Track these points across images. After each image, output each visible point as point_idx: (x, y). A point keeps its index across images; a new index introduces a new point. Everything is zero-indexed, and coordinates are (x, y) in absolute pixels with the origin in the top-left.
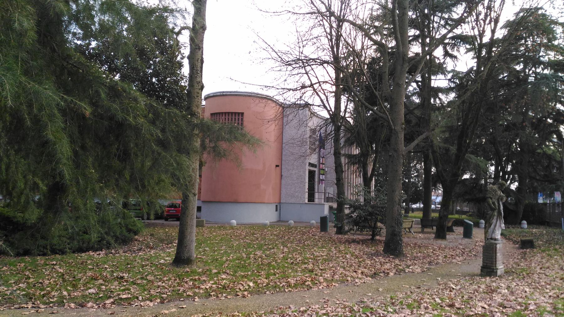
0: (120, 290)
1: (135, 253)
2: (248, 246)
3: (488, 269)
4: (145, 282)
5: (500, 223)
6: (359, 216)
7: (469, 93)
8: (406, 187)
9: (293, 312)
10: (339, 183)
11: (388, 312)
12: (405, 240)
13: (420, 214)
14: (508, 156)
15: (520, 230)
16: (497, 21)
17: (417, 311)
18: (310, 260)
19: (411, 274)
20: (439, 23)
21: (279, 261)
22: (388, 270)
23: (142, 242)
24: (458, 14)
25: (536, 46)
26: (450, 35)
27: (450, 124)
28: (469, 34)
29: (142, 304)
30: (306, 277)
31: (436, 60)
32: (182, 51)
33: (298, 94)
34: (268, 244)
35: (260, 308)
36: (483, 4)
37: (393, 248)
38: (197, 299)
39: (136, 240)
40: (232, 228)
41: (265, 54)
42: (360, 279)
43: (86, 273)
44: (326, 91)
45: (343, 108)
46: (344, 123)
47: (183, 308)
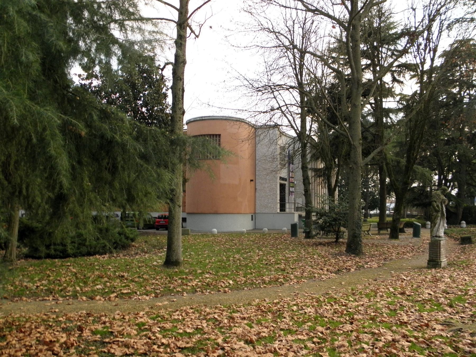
0: (122, 287)
1: (133, 257)
2: (228, 250)
3: (434, 262)
4: (141, 280)
5: (443, 223)
6: (325, 222)
7: (414, 112)
8: (364, 196)
9: (267, 304)
10: (307, 193)
11: (349, 301)
12: (364, 241)
13: (377, 219)
14: (448, 166)
15: (460, 229)
16: (435, 50)
17: (374, 299)
18: (282, 261)
19: (369, 269)
20: (387, 54)
21: (255, 262)
22: (349, 266)
23: (138, 248)
24: (402, 46)
25: (469, 72)
26: (396, 64)
27: (400, 140)
28: (412, 62)
29: (140, 297)
30: (279, 275)
31: (386, 85)
32: (167, 83)
33: (268, 116)
34: (245, 249)
35: (239, 301)
36: (423, 36)
37: (354, 248)
38: (185, 294)
39: (133, 246)
40: (214, 235)
41: (238, 83)
42: (326, 275)
43: (94, 272)
44: (293, 113)
45: (308, 128)
46: (309, 141)
47: (173, 301)
